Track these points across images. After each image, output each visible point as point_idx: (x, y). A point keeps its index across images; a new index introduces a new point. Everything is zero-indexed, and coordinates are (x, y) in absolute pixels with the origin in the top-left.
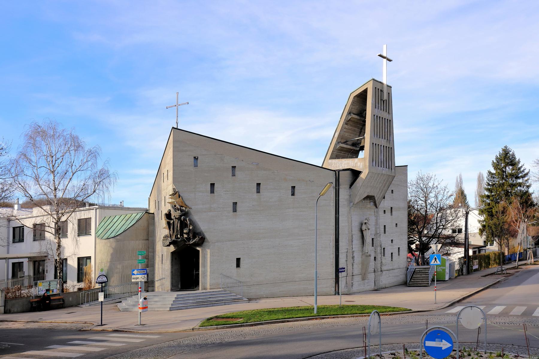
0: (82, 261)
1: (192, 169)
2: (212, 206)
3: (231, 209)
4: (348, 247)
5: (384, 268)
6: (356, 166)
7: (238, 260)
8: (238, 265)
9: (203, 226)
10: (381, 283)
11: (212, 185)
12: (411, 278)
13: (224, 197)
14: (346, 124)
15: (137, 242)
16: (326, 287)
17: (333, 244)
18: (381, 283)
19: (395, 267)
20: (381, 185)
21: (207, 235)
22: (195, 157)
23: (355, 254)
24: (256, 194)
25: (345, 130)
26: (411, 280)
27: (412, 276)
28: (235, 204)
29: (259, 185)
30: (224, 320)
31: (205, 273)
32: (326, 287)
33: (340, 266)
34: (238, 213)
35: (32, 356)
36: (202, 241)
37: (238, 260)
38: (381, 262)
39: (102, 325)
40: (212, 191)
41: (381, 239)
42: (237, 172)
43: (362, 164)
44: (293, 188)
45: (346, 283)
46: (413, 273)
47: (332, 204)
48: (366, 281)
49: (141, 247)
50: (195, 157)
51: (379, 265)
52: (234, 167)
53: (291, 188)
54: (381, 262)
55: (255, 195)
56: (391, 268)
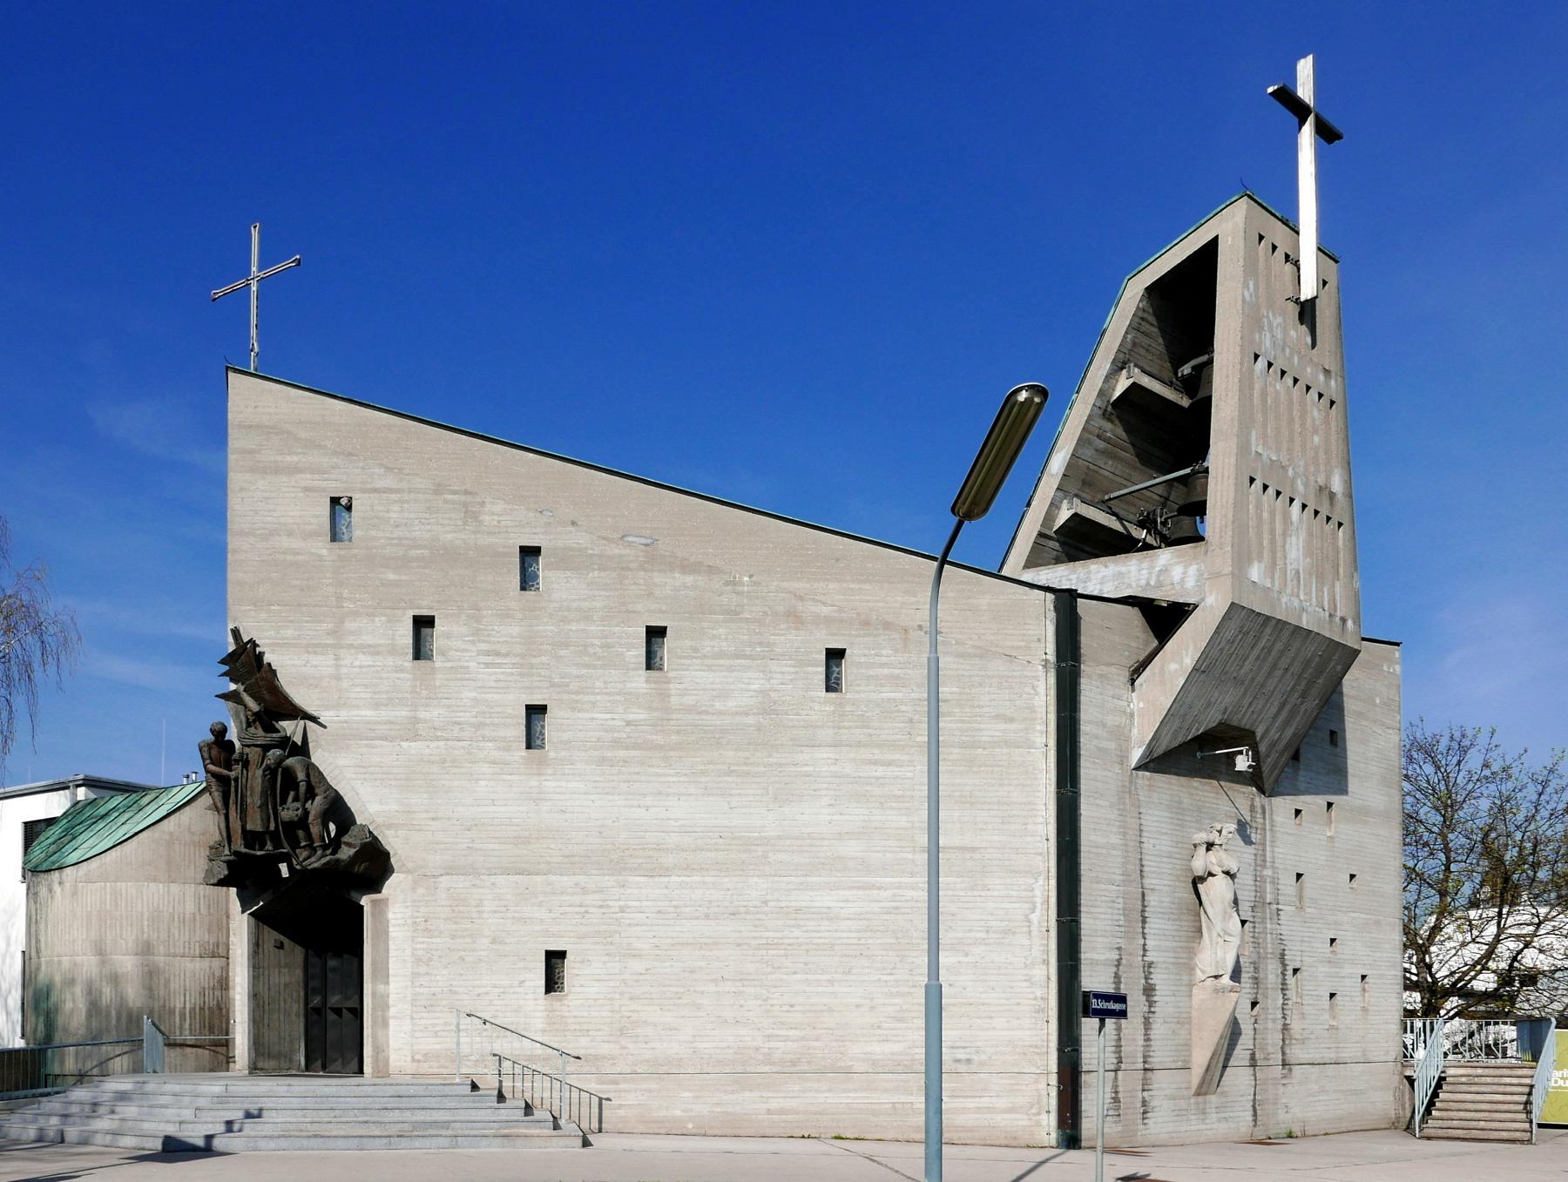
2: (422, 714)
3: (517, 730)
4: (1122, 943)
5: (1296, 1053)
6: (1160, 585)
7: (554, 959)
8: (552, 983)
9: (371, 806)
10: (1282, 1116)
11: (423, 624)
12: (1431, 1104)
13: (482, 672)
14: (1105, 415)
15: (175, 888)
16: (1011, 1110)
17: (1046, 889)
18: (1282, 1116)
22: (335, 501)
23: (1157, 978)
25: (1101, 444)
26: (1428, 1111)
27: (1435, 1095)
28: (535, 712)
29: (655, 634)
30: (1475, 1134)
32: (1011, 1110)
33: (1094, 979)
34: (550, 751)
36: (374, 865)
37: (554, 959)
38: (1285, 1028)
40: (419, 651)
41: (1284, 930)
42: (543, 568)
43: (1193, 570)
45: (1116, 1100)
46: (1439, 1086)
47: (1040, 740)
48: (1213, 1098)
49: (190, 907)
50: (335, 501)
51: (1275, 1038)
52: (530, 553)
54: (1285, 1028)
55: (640, 680)
56: (1330, 1055)
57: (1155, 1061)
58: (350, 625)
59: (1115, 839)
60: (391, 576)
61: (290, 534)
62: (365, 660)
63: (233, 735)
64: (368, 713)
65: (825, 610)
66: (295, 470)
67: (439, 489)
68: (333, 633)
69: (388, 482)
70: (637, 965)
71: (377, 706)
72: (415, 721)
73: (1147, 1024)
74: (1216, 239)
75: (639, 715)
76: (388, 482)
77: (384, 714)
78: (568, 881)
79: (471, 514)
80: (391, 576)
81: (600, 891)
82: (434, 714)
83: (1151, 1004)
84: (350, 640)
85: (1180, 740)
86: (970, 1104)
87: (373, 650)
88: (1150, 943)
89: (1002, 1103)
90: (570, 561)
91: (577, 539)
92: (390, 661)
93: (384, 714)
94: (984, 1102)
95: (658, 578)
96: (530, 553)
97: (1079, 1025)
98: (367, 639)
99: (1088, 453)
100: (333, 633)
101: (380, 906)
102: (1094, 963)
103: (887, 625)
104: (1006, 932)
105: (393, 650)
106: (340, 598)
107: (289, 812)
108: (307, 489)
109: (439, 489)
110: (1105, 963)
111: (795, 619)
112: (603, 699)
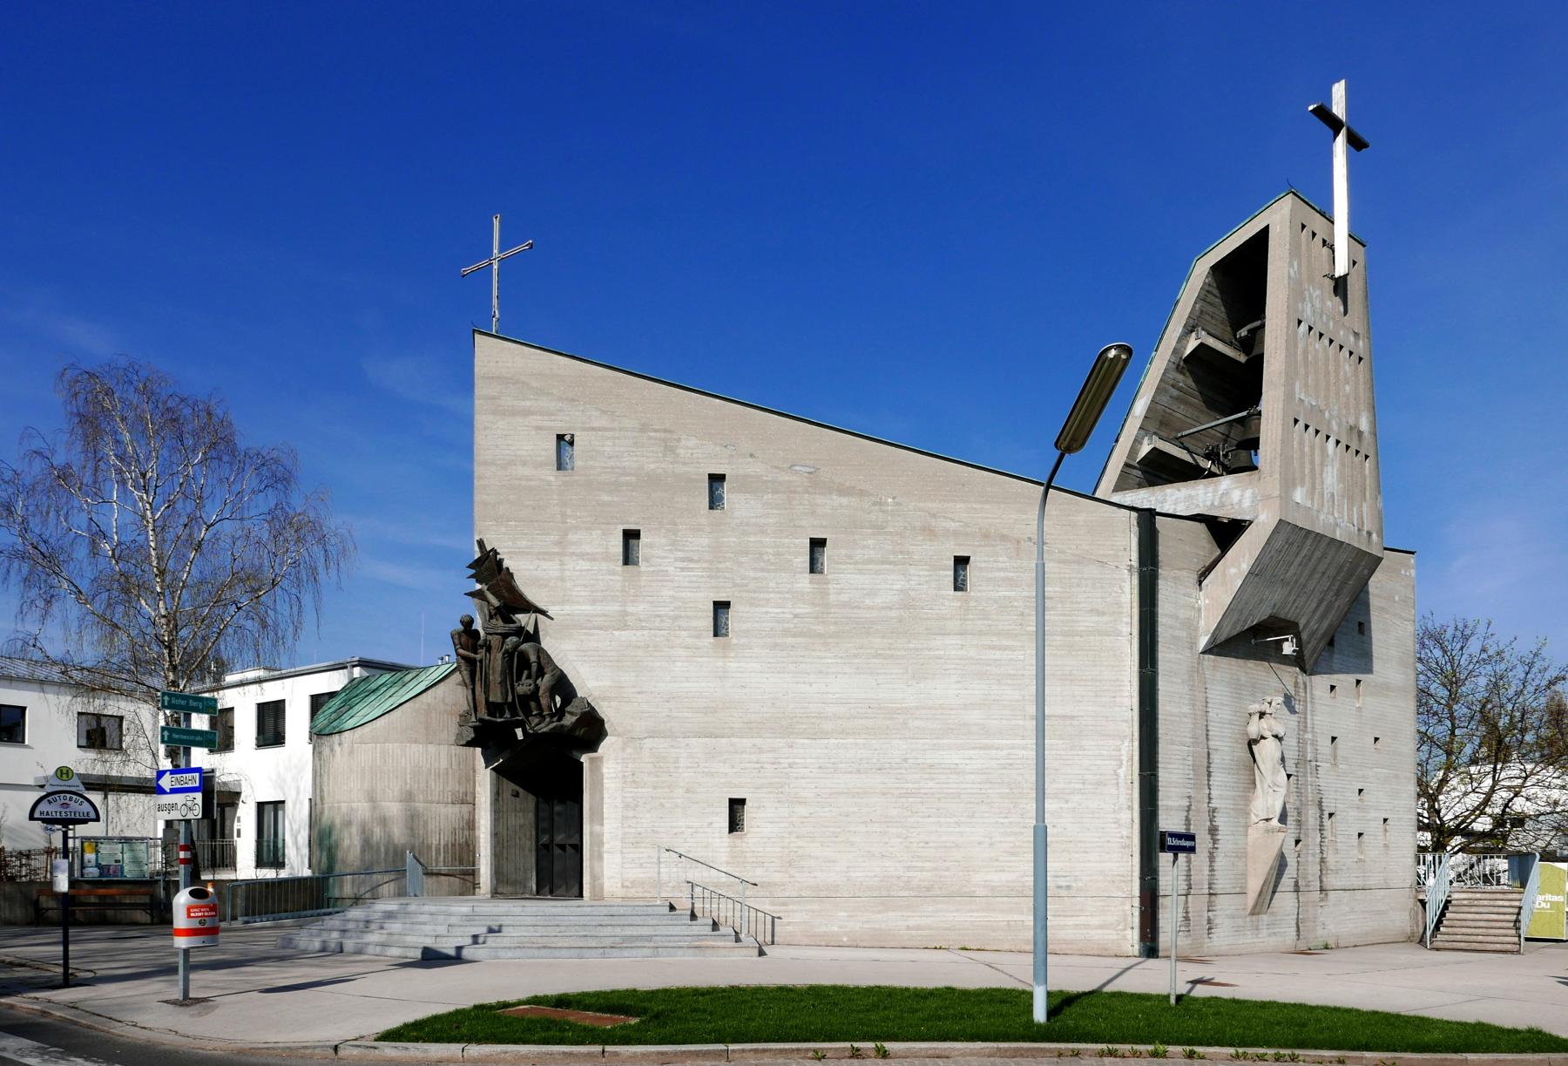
0: (269, 811)
1: (550, 474)
2: (630, 609)
5: (1331, 881)
6: (1222, 505)
7: (736, 805)
8: (735, 824)
10: (1320, 932)
11: (631, 536)
12: (1439, 922)
13: (678, 574)
14: (1178, 369)
15: (431, 748)
16: (1101, 927)
17: (1129, 770)
18: (1320, 932)
19: (1371, 882)
20: (1326, 583)
21: (605, 711)
22: (560, 437)
23: (1220, 821)
24: (807, 575)
25: (1175, 393)
26: (1437, 928)
27: (1443, 914)
28: (721, 607)
29: (817, 544)
31: (598, 842)
32: (1101, 927)
34: (733, 638)
35: (915, 1055)
37: (736, 805)
38: (1322, 860)
39: (67, 981)
43: (1248, 493)
44: (961, 562)
45: (1187, 918)
46: (1446, 907)
48: (1265, 918)
50: (560, 437)
52: (716, 479)
53: (952, 563)
54: (1322, 860)
55: (805, 581)
57: (1218, 888)
58: (572, 537)
59: (1186, 709)
60: (606, 498)
61: (524, 464)
62: (584, 565)
63: (478, 625)
64: (587, 608)
65: (953, 525)
66: (528, 412)
67: (644, 428)
68: (559, 543)
69: (603, 422)
70: (802, 810)
71: (594, 602)
72: (625, 613)
73: (1212, 858)
74: (1266, 230)
75: (803, 609)
76: (603, 422)
77: (599, 608)
78: (746, 742)
79: (669, 449)
80: (606, 498)
81: (773, 750)
82: (639, 608)
83: (1215, 841)
84: (573, 549)
85: (1238, 630)
86: (1070, 921)
87: (591, 557)
88: (1214, 793)
89: (1095, 921)
90: (749, 486)
91: (755, 468)
92: (604, 566)
93: (599, 608)
94: (1081, 920)
95: (819, 500)
96: (716, 479)
97: (1157, 858)
98: (587, 549)
99: (1165, 399)
100: (559, 543)
101: (596, 763)
102: (1169, 808)
103: (1003, 538)
104: (1099, 783)
105: (607, 557)
106: (564, 515)
107: (524, 687)
108: (538, 428)
109: (644, 428)
110: (1178, 809)
111: (929, 532)
112: (775, 596)
